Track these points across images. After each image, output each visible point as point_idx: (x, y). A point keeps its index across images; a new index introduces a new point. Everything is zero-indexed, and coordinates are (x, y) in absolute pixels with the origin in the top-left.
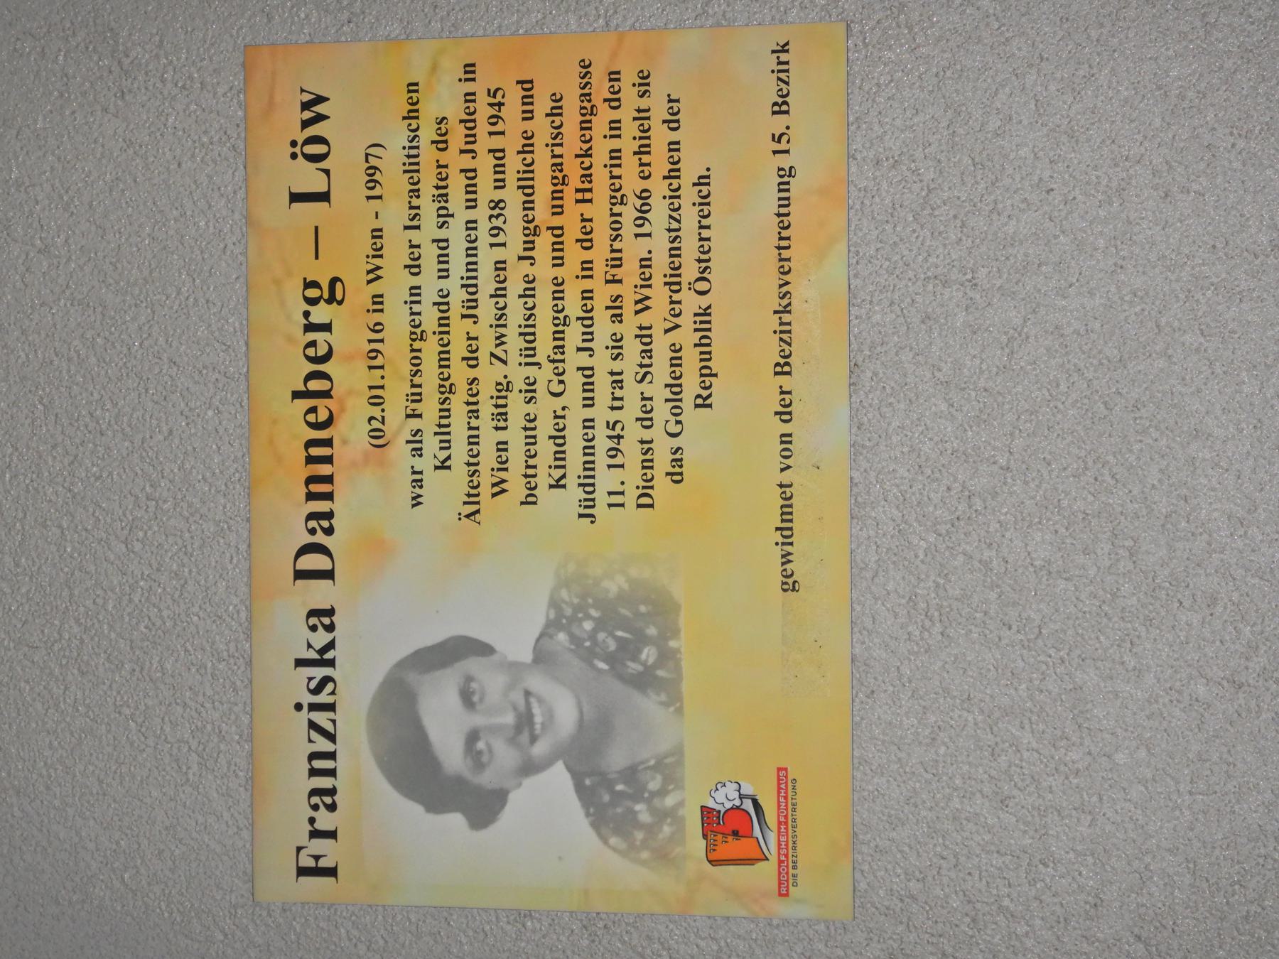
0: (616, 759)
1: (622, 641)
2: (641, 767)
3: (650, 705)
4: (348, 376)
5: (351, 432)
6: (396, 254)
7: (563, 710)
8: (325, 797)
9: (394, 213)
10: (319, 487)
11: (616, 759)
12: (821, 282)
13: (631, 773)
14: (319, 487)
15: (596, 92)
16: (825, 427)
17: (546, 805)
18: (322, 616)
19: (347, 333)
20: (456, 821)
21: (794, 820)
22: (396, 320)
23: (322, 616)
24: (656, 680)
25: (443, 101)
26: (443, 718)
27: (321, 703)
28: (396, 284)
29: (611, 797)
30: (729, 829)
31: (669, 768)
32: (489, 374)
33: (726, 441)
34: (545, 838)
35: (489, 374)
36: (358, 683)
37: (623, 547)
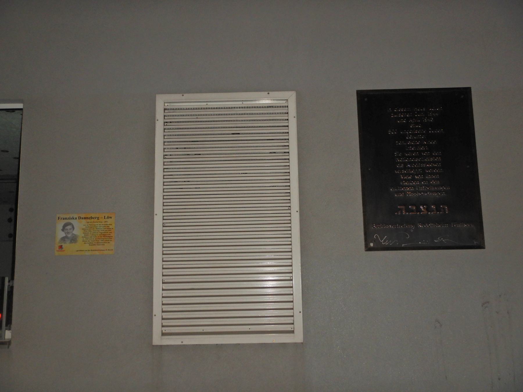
0: (66, 239)
1: (74, 240)
2: (438, 177)
3: (69, 242)
4: (92, 220)
5: (89, 220)
6: (100, 223)
7: (69, 236)
8: (64, 219)
9: (103, 223)
10: (85, 218)
11: (66, 239)
12: (97, 253)
13: (65, 240)
14: (85, 218)
15: (110, 237)
16: (87, 253)
17: (62, 234)
18: (76, 219)
19: (96, 220)
20: (61, 228)
21: (11, 289)
22: (96, 224)
23: (76, 219)
24: (71, 242)
25: (111, 227)
26: (69, 227)
27: (70, 218)
28: (98, 223)
29: (63, 239)
30: (61, 247)
31: (65, 243)
32: (92, 230)
33: (87, 247)
34: (61, 234)
35: (92, 230)
36: (72, 221)
37: (80, 240)
